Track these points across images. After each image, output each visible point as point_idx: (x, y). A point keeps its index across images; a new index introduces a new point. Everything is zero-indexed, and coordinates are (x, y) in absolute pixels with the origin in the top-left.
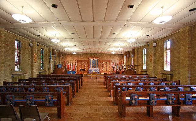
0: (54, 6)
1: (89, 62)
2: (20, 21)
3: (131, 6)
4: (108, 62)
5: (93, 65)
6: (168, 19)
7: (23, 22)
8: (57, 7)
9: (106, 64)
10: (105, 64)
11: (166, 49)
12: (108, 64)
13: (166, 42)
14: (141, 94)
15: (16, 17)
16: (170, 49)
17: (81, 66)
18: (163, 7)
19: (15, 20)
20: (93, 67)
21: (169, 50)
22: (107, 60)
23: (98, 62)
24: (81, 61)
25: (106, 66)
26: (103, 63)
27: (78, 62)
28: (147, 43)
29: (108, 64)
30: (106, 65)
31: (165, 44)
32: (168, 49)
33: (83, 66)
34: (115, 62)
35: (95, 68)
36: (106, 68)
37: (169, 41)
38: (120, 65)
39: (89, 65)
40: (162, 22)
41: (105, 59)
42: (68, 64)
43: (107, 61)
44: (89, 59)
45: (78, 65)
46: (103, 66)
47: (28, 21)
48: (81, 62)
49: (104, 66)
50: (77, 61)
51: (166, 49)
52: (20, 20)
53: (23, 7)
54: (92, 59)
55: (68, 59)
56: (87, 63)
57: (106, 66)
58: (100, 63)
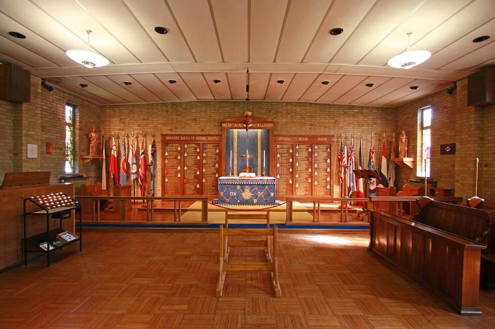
0: (160, 30)
1: (223, 144)
2: (83, 64)
3: (337, 31)
4: (319, 143)
5: (241, 157)
6: (420, 57)
7: (89, 66)
8: (166, 33)
9: (311, 154)
10: (302, 153)
11: (422, 128)
12: (320, 153)
13: (423, 110)
14: (321, 201)
15: (76, 56)
16: (431, 127)
17: (183, 163)
18: (411, 33)
19: (73, 61)
20: (242, 169)
21: (429, 131)
22: (316, 137)
23: (268, 145)
24: (184, 140)
25: (311, 164)
26: (293, 147)
27: (165, 143)
28: (448, 83)
29: (320, 153)
30: (311, 160)
31: (419, 114)
32: (427, 128)
33: (190, 161)
34: (356, 143)
35: (253, 175)
36: (311, 175)
37: (429, 108)
38: (384, 161)
39: (221, 161)
40: (410, 64)
41: (307, 131)
42: (114, 153)
43: (312, 141)
44: (222, 129)
45: (164, 157)
46: (292, 165)
47: (101, 62)
48: (182, 143)
49: (301, 165)
50: (158, 139)
51: (422, 128)
52: (83, 62)
53: (89, 32)
54: (235, 131)
55: (115, 127)
56: (211, 151)
57: (311, 164)
58: (281, 151)
